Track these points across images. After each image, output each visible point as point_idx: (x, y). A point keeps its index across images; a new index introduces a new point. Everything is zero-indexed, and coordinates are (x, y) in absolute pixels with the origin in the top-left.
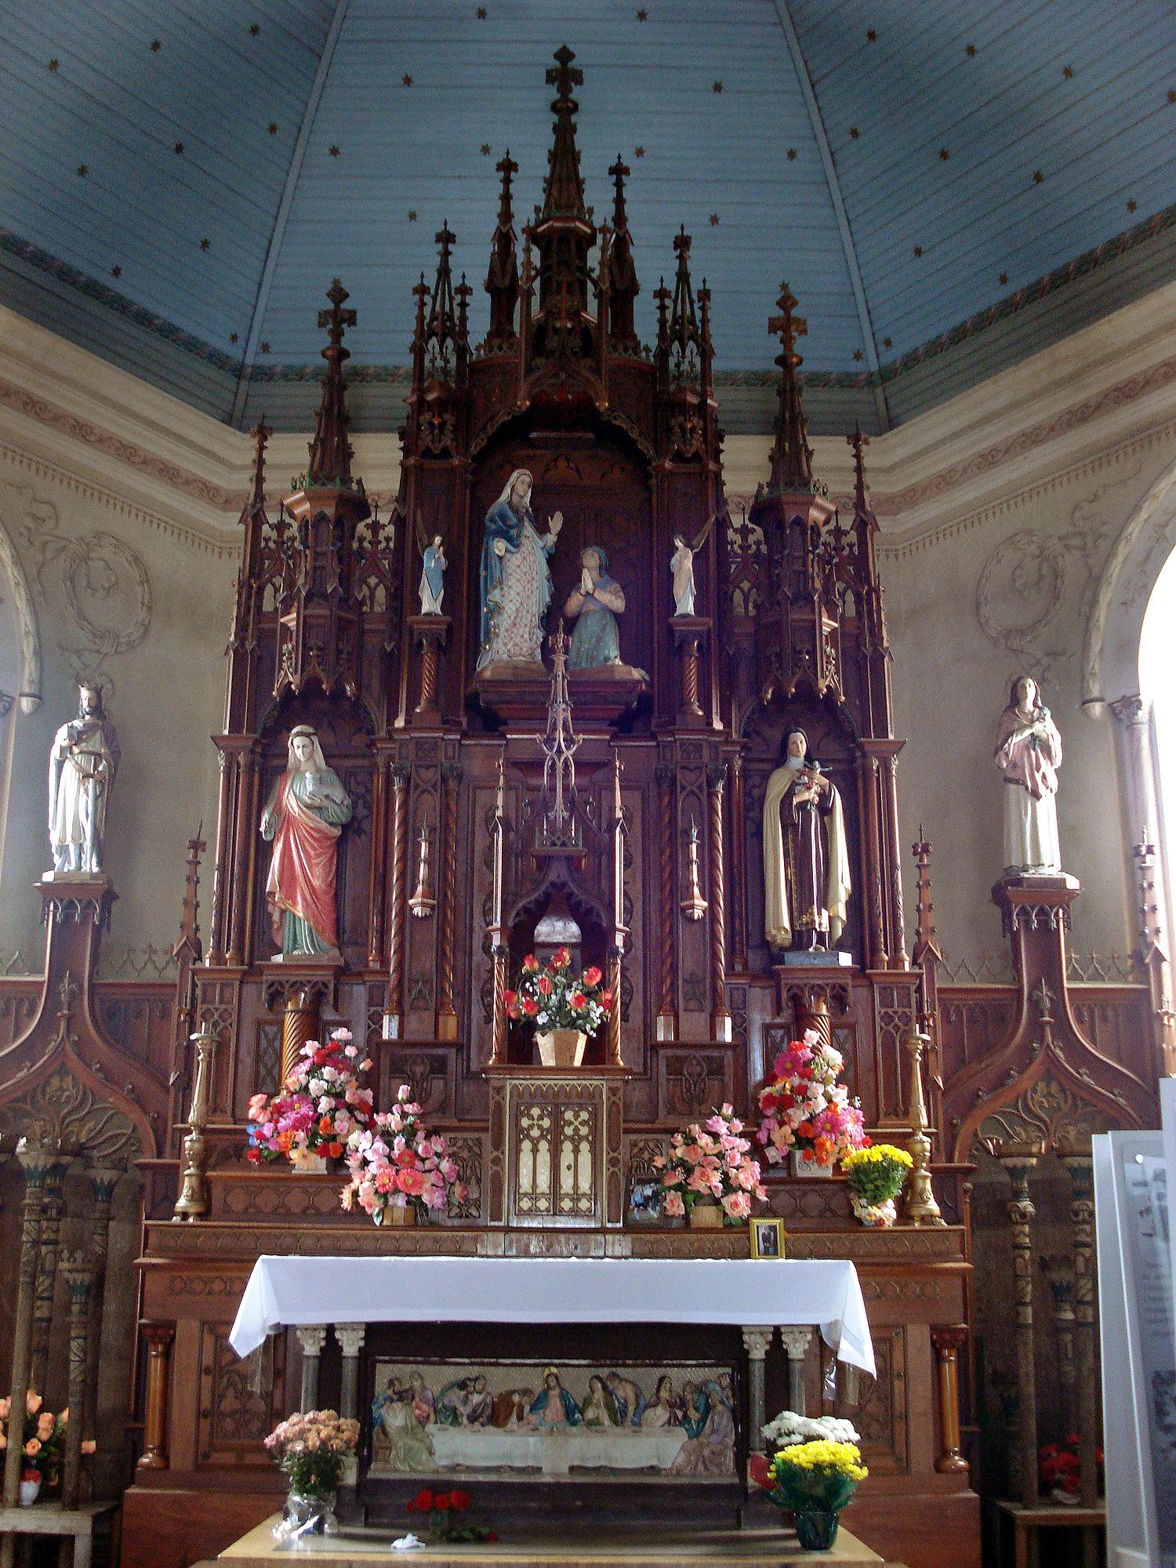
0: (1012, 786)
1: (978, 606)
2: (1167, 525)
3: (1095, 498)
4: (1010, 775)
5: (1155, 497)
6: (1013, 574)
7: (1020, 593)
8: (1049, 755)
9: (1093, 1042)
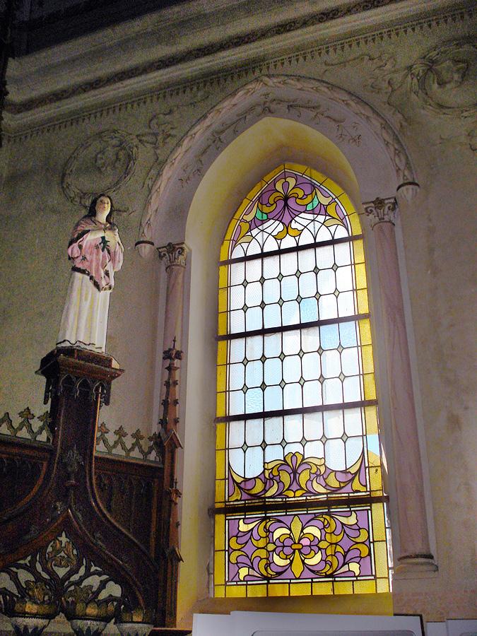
0: (78, 275)
1: (64, 175)
2: (222, 132)
3: (171, 112)
4: (78, 264)
5: (219, 111)
6: (96, 156)
7: (99, 169)
8: (113, 259)
9: (109, 511)
